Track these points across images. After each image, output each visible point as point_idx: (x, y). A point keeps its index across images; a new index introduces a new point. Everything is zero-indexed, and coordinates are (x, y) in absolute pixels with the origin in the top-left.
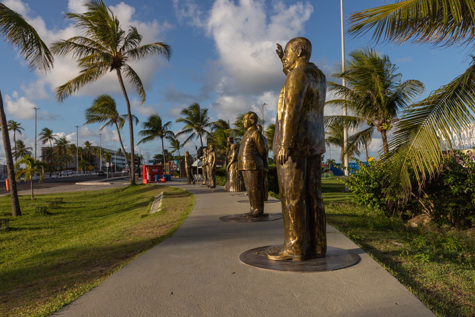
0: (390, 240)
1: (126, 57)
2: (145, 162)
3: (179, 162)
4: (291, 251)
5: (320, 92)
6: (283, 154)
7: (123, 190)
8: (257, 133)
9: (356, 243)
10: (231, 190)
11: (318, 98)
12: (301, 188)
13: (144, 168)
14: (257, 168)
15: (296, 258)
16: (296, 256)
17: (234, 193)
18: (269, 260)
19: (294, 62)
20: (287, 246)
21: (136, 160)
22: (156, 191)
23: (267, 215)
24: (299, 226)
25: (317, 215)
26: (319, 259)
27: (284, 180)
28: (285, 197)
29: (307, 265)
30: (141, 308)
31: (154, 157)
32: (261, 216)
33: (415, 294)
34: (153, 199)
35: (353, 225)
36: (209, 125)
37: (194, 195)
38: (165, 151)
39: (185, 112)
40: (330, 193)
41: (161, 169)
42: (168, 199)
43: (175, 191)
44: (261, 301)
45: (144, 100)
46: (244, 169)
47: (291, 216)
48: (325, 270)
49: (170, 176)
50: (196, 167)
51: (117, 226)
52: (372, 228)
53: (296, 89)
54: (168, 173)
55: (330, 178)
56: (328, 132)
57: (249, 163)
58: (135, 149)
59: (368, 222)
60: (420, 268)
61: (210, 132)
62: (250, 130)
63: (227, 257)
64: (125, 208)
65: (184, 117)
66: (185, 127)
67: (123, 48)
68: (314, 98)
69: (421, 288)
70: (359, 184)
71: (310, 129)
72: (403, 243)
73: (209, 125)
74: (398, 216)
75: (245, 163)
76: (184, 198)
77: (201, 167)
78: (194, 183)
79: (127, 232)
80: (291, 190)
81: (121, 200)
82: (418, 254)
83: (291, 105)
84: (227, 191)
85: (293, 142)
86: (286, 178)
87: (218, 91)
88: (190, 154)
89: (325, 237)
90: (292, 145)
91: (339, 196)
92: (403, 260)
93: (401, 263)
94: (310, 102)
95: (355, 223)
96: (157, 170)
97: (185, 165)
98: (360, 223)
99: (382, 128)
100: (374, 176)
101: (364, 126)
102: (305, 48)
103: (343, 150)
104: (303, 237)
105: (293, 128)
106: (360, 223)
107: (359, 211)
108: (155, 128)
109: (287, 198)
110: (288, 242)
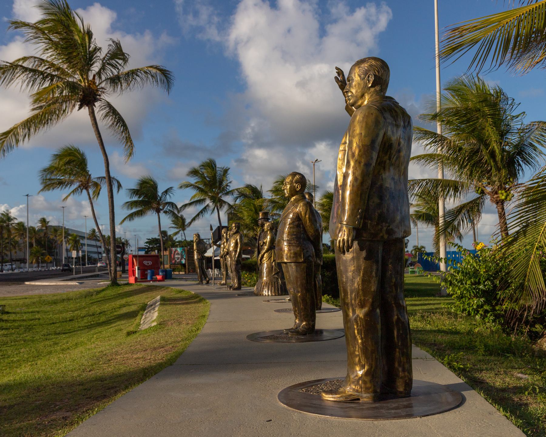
0: (510, 370)
1: (102, 88)
2: (132, 250)
3: (184, 250)
5: (402, 142)
6: (345, 238)
7: (98, 292)
8: (304, 205)
9: (458, 375)
10: (265, 292)
11: (399, 151)
12: (372, 290)
15: (366, 398)
16: (365, 395)
17: (270, 298)
18: (323, 400)
19: (363, 96)
20: (352, 380)
21: (118, 247)
22: (150, 294)
23: (321, 332)
25: (398, 332)
26: (400, 400)
27: (347, 277)
28: (347, 304)
29: (382, 408)
31: (147, 243)
32: (311, 333)
34: (144, 308)
35: (453, 347)
37: (208, 301)
38: (164, 233)
39: (194, 172)
41: (157, 262)
42: (168, 307)
43: (179, 295)
45: (131, 154)
46: (285, 261)
47: (358, 333)
48: (410, 416)
49: (171, 272)
50: (211, 258)
51: (89, 349)
52: (481, 351)
53: (365, 136)
54: (167, 266)
55: (417, 274)
56: (415, 204)
57: (292, 251)
59: (476, 342)
61: (232, 203)
62: (295, 200)
64: (101, 321)
65: (193, 180)
66: (194, 196)
68: (394, 152)
71: (386, 199)
72: (530, 374)
75: (286, 252)
76: (193, 305)
77: (218, 258)
78: (208, 283)
80: (358, 293)
81: (96, 309)
83: (358, 162)
84: (258, 294)
85: (361, 218)
86: (350, 274)
87: (244, 141)
88: (202, 237)
90: (359, 224)
91: (431, 302)
92: (531, 400)
93: (527, 405)
94: (387, 157)
95: (456, 344)
96: (150, 263)
98: (464, 344)
99: (498, 197)
100: (487, 271)
101: (470, 195)
102: (379, 75)
107: (462, 326)
108: (147, 197)
109: (352, 305)
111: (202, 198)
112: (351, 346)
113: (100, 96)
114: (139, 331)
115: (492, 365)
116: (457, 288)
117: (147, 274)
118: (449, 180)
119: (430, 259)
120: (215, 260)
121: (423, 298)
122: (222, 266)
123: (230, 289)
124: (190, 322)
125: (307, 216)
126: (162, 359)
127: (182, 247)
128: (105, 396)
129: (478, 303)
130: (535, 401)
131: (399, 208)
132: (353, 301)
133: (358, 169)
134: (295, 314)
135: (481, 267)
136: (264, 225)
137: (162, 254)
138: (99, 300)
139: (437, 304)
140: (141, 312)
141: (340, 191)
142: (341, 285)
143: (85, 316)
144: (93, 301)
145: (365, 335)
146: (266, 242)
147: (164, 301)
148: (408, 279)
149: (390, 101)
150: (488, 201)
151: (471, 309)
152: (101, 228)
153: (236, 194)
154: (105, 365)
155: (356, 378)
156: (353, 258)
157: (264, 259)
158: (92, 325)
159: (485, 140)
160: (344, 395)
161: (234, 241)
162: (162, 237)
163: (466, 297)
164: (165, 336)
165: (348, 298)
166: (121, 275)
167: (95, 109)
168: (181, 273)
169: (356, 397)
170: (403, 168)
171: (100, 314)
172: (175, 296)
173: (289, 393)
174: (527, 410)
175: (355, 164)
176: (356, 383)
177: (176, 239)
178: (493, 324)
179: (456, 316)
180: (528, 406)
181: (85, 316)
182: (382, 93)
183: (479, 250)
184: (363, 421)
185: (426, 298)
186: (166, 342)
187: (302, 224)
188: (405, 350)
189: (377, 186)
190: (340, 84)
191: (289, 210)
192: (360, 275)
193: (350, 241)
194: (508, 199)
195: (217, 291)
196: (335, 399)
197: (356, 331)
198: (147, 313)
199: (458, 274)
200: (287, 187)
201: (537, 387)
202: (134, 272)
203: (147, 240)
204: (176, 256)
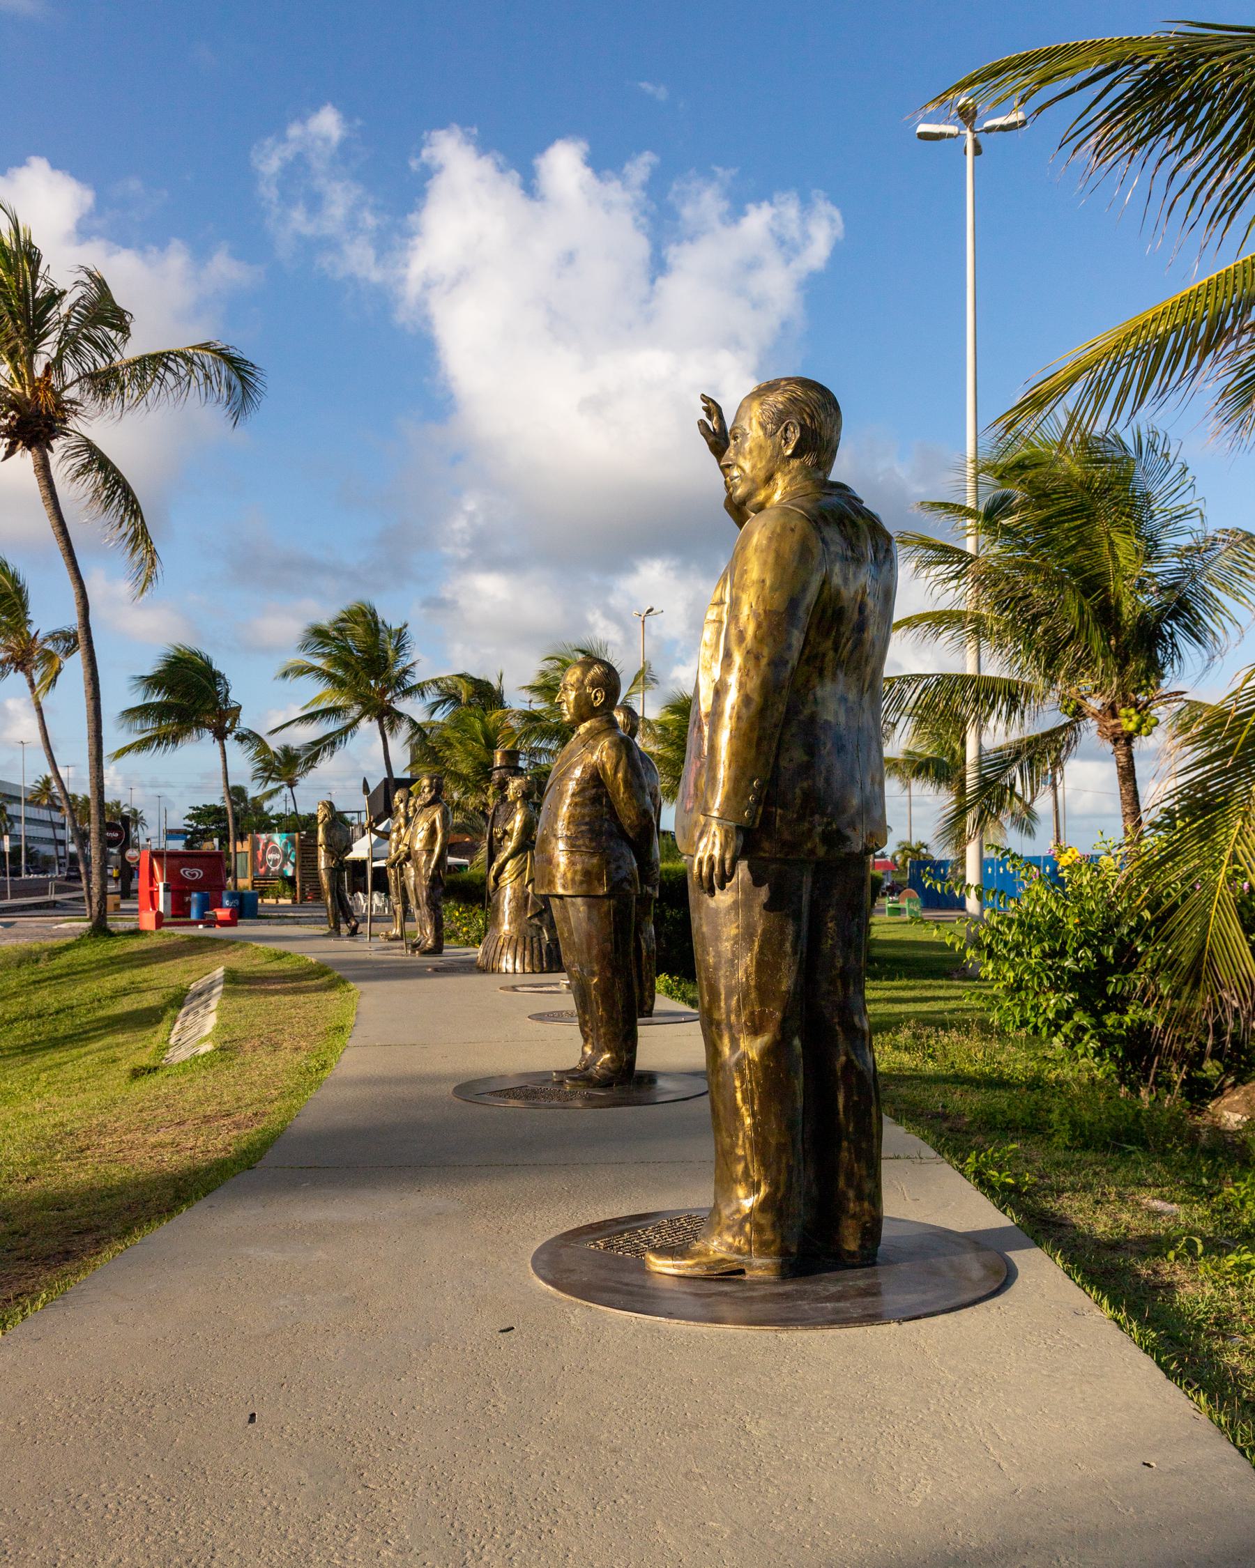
0: (1132, 1189)
1: (72, 402)
2: (149, 836)
3: (292, 841)
4: (740, 1242)
5: (870, 602)
6: (717, 853)
7: (55, 953)
8: (614, 745)
9: (1001, 1206)
10: (507, 963)
11: (861, 627)
12: (783, 988)
13: (144, 867)
14: (609, 891)
15: (761, 1268)
16: (758, 1262)
17: (519, 979)
18: (649, 1273)
19: (769, 478)
20: (725, 1221)
21: (111, 827)
22: (196, 961)
23: (649, 1078)
24: (773, 1141)
25: (847, 1098)
26: (849, 1273)
27: (718, 954)
28: (718, 1024)
29: (802, 1295)
30: (121, 1485)
31: (190, 817)
32: (626, 1082)
33: (1220, 1425)
34: (179, 1000)
35: (995, 1126)
36: (418, 690)
37: (352, 985)
38: (237, 793)
39: (319, 634)
40: (904, 982)
41: (218, 866)
42: (244, 1002)
43: (275, 966)
44: (613, 1451)
45: (149, 579)
46: (560, 891)
47: (744, 1100)
48: (873, 1318)
49: (254, 898)
50: (364, 862)
51: (26, 1116)
52: (1062, 1139)
53: (773, 589)
54: (245, 883)
55: (907, 917)
56: (901, 740)
57: (579, 867)
58: (106, 782)
59: (1050, 1111)
60: (1245, 1312)
61: (420, 718)
62: (589, 731)
63: (477, 1257)
64: (60, 1034)
66: (318, 700)
67: (55, 365)
68: (846, 630)
69: (1245, 1395)
70: (1019, 954)
71: (824, 752)
72: (1183, 1202)
73: (418, 690)
74: (1169, 1086)
75: (562, 868)
76: (314, 996)
77: (381, 863)
78: (354, 932)
79: (67, 1142)
80: (746, 995)
81: (45, 998)
82: (1239, 1254)
83: (753, 656)
84: (486, 968)
85: (758, 802)
86: (726, 946)
87: (448, 551)
88: (339, 807)
89: (878, 1186)
90: (753, 817)
91: (941, 993)
92: (1182, 1275)
93: (1170, 1287)
94: (829, 644)
95: (999, 1117)
96: (199, 873)
97: (315, 852)
98: (1019, 1115)
99: (1119, 725)
100: (1082, 924)
101: (1048, 716)
102: (811, 420)
103: (961, 792)
104: (789, 1187)
105: (758, 744)
106: (1019, 1115)
107: (1015, 1061)
108: (189, 696)
109: (730, 1027)
110: (730, 1201)
111: (339, 703)
112: (724, 1134)
113: (65, 421)
114: (164, 1067)
115: (1086, 1176)
116: (1007, 965)
117: (189, 902)
118: (995, 679)
119: (939, 886)
120: (376, 870)
121: (919, 982)
122: (393, 890)
123: (413, 952)
124: (303, 1044)
125: (620, 775)
126: (225, 1149)
127: (287, 832)
128: (68, 1252)
129: (1059, 1006)
130: (1192, 1276)
131: (858, 776)
132: (733, 1017)
133: (752, 673)
134: (582, 1031)
135: (1068, 913)
136: (507, 783)
137: (231, 850)
138: (55, 973)
139: (956, 998)
140: (171, 1012)
141: (706, 729)
142: (703, 975)
143: (16, 1020)
144: (40, 976)
145: (761, 1104)
146: (512, 830)
147: (233, 979)
148: (881, 928)
149: (840, 495)
150: (1090, 730)
151: (1040, 1020)
152: (63, 773)
153: (432, 696)
154: (70, 1163)
155: (737, 1216)
156: (735, 902)
157: (506, 875)
158: (35, 1043)
159: (1086, 578)
160: (704, 1260)
161: (426, 826)
162: (233, 803)
163: (1027, 988)
164: (236, 1084)
165: (719, 1008)
166: (117, 905)
167: (50, 454)
168: (282, 901)
169: (736, 1267)
170: (869, 670)
171: (57, 1013)
172: (264, 967)
173: (562, 1251)
174: (1172, 1302)
175: (746, 660)
176: (735, 1229)
177: (271, 809)
178: (1097, 1059)
179: (1001, 1033)
180: (1174, 1291)
181: (16, 1020)
182: (821, 474)
183: (1068, 867)
184: (751, 1333)
185: (927, 982)
186: (238, 1099)
187: (607, 796)
188: (864, 1145)
189: (801, 717)
190: (712, 439)
191: (571, 757)
192: (751, 950)
193: (727, 866)
194: (1144, 731)
195: (375, 956)
196: (681, 1272)
197: (739, 1096)
198: (187, 1014)
199: (1010, 929)
200: (567, 696)
201: (1198, 1241)
202: (153, 897)
203: (191, 811)
204: (270, 856)
